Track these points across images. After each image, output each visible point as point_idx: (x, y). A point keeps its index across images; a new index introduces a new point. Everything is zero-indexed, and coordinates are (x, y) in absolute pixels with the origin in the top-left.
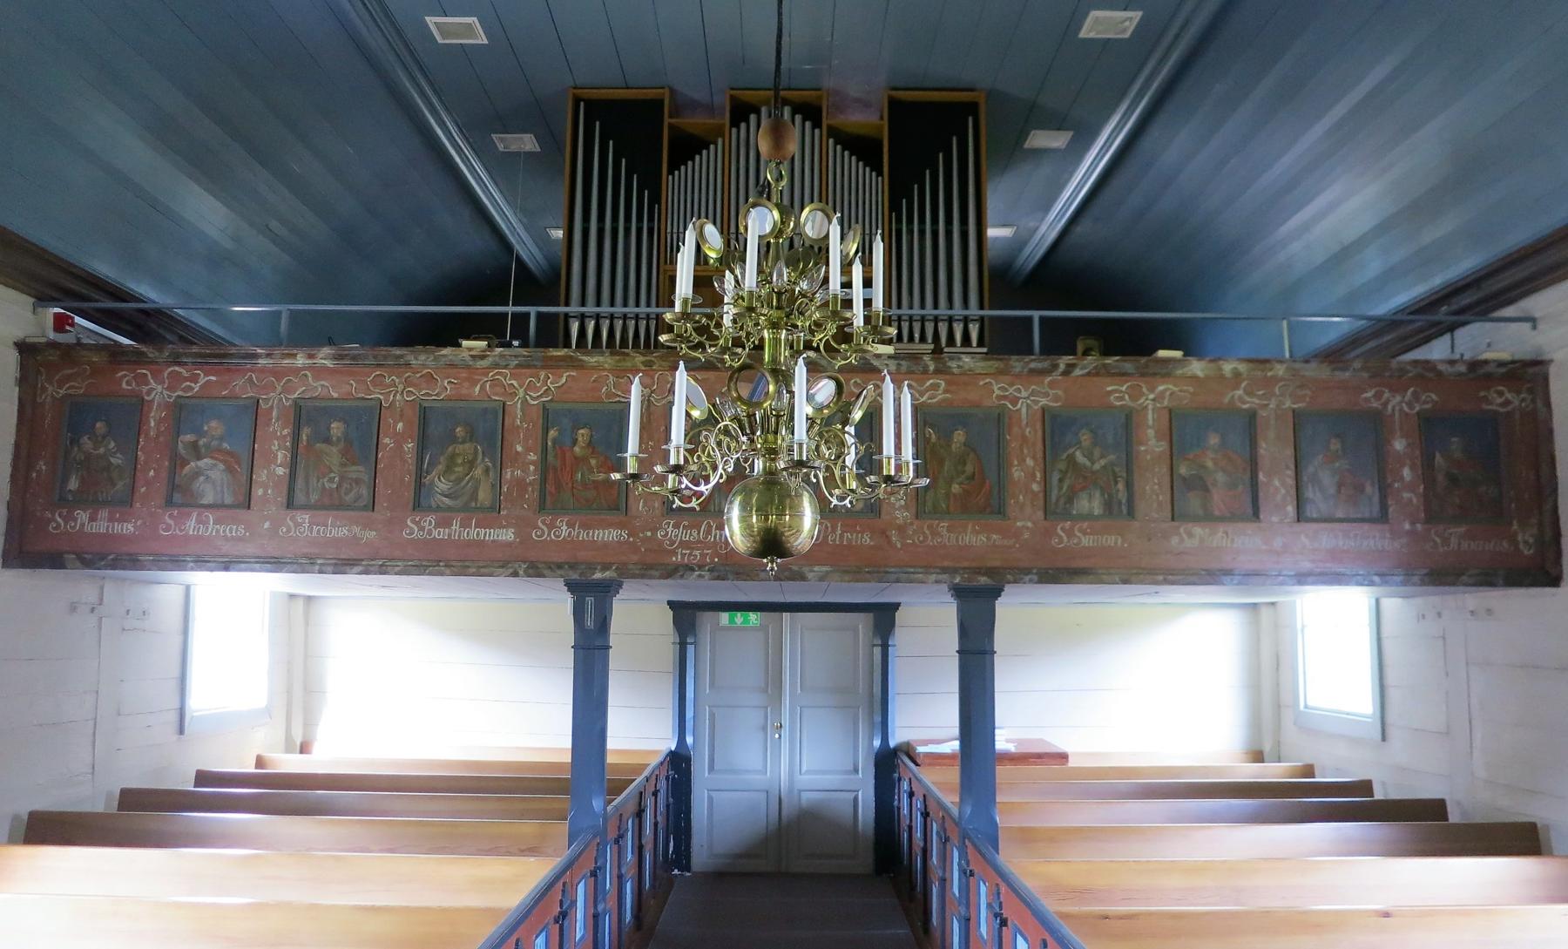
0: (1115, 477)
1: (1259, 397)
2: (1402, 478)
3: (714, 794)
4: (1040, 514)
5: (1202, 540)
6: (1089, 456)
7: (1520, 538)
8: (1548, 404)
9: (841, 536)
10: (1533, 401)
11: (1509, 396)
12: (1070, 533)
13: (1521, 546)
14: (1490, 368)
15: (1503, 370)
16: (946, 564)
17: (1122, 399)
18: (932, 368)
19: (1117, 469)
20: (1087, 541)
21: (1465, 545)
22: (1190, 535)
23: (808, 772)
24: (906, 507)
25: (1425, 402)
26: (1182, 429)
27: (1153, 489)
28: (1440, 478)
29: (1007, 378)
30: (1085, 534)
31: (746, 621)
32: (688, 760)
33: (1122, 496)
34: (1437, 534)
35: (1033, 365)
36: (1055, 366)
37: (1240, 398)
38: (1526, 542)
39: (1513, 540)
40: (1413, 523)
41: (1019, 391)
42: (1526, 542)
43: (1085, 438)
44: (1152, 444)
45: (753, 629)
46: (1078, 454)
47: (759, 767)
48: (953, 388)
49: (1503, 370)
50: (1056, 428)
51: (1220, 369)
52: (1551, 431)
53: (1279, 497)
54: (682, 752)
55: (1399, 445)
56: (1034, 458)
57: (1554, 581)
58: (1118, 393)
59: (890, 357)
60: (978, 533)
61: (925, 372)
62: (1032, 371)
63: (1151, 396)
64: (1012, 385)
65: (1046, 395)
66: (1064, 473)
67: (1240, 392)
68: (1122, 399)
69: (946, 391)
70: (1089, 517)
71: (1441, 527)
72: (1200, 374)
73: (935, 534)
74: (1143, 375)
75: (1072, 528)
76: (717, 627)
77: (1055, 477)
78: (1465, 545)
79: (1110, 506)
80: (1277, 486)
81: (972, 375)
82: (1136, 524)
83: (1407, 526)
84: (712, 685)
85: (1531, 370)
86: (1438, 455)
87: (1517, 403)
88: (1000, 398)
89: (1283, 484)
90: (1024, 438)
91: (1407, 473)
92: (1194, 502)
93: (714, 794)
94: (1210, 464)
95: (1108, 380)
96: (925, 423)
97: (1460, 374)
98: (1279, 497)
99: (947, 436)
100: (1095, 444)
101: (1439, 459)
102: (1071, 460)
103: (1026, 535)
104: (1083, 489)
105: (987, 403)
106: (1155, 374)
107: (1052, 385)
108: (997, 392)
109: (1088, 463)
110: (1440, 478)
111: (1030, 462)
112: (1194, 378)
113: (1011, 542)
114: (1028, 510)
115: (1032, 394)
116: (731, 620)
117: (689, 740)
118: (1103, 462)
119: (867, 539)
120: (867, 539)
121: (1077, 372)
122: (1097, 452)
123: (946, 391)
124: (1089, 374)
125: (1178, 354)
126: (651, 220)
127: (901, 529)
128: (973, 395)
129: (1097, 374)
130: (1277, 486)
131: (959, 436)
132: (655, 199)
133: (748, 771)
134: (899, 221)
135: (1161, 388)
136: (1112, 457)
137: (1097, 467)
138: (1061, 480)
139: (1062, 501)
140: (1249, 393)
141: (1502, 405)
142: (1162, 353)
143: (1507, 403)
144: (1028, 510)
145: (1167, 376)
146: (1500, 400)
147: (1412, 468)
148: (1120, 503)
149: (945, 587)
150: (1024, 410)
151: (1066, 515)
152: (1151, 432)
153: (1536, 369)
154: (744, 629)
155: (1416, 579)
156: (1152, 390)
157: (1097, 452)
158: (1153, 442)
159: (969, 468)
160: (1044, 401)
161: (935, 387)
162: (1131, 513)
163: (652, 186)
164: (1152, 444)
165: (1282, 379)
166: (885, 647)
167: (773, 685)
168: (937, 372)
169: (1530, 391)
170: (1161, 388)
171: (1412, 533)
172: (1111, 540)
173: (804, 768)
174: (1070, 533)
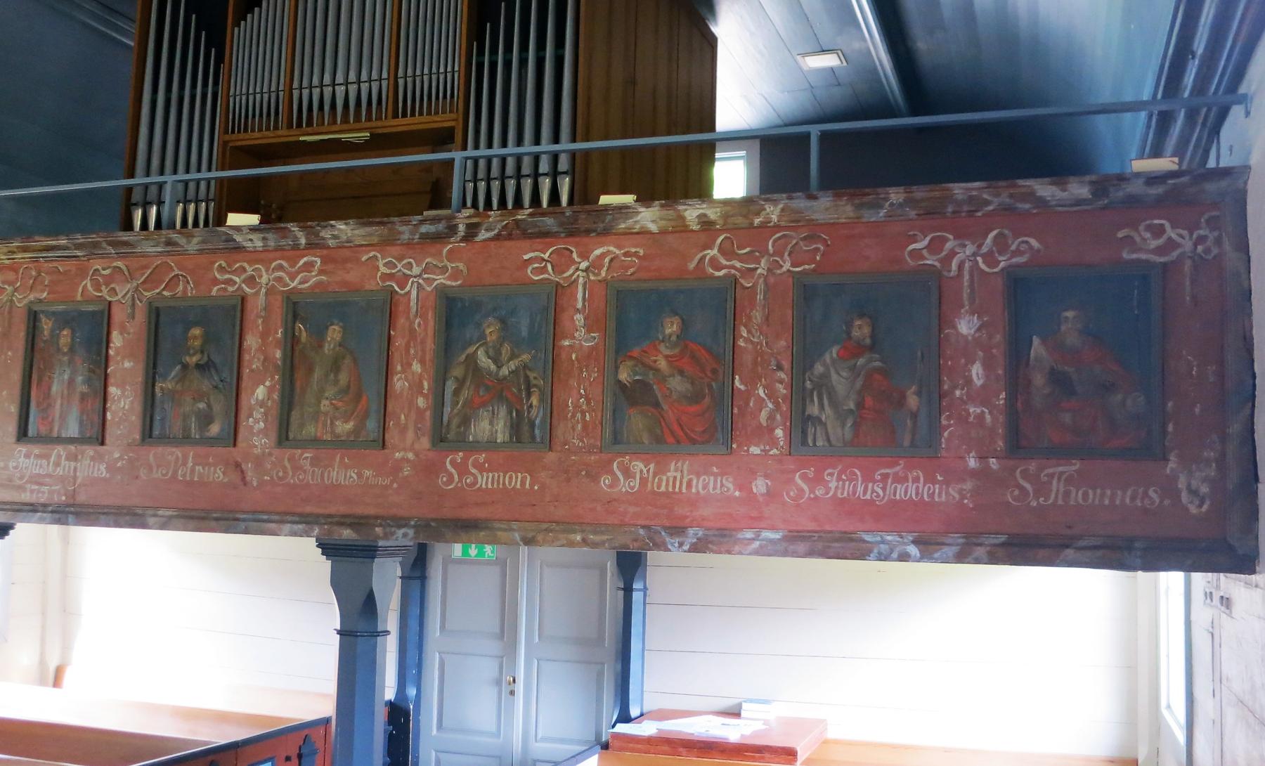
0: (529, 387)
1: (741, 259)
2: (969, 381)
3: (442, 756)
4: (425, 442)
5: (643, 481)
6: (496, 360)
7: (1182, 483)
8: (1243, 247)
9: (193, 471)
10: (1218, 242)
11: (1171, 233)
12: (462, 470)
13: (1184, 497)
14: (1136, 188)
15: (1158, 190)
16: (308, 509)
17: (543, 270)
18: (303, 241)
19: (532, 375)
20: (484, 481)
21: (1077, 496)
22: (628, 474)
23: (544, 739)
24: (264, 432)
25: (1018, 253)
26: (631, 312)
27: (582, 400)
28: (1039, 380)
29: (395, 250)
30: (481, 468)
31: (481, 553)
32: (406, 714)
33: (537, 414)
34: (1025, 475)
35: (424, 229)
36: (453, 229)
37: (713, 259)
38: (1193, 492)
39: (1170, 490)
40: (982, 458)
41: (410, 266)
42: (1193, 492)
43: (491, 330)
44: (580, 336)
45: (488, 563)
46: (481, 353)
47: (493, 729)
48: (330, 267)
49: (1158, 190)
50: (454, 313)
51: (683, 218)
52: (1247, 295)
53: (764, 415)
54: (403, 705)
55: (966, 326)
56: (422, 362)
57: (1242, 562)
58: (537, 263)
59: (253, 229)
60: (347, 467)
61: (296, 247)
62: (424, 237)
63: (584, 265)
64: (400, 259)
65: (444, 270)
66: (461, 383)
67: (714, 252)
68: (543, 270)
69: (321, 272)
70: (491, 445)
71: (1033, 466)
72: (653, 228)
73: (297, 468)
74: (571, 234)
75: (465, 459)
76: (448, 561)
77: (450, 386)
78: (1077, 496)
79: (518, 429)
80: (765, 401)
81: (347, 245)
82: (551, 457)
83: (972, 463)
84: (443, 627)
85: (1211, 187)
86: (1036, 341)
87: (1188, 245)
88: (386, 277)
89: (771, 395)
90: (412, 331)
91: (976, 371)
92: (637, 421)
93: (442, 756)
94: (662, 364)
95: (526, 244)
96: (295, 317)
97: (1079, 202)
98: (764, 415)
99: (319, 334)
100: (501, 340)
101: (1037, 348)
102: (472, 359)
103: (407, 471)
104: (484, 404)
105: (370, 285)
106: (588, 232)
107: (452, 255)
108: (383, 269)
109: (493, 367)
110: (1039, 380)
111: (416, 367)
112: (644, 232)
113: (387, 482)
114: (410, 435)
115: (425, 271)
116: (464, 552)
117: (411, 692)
118: (512, 365)
119: (218, 475)
120: (218, 475)
121: (483, 235)
122: (506, 350)
123: (321, 272)
124: (497, 238)
125: (628, 199)
126: (216, 83)
127: (259, 462)
128: (352, 275)
129: (510, 237)
130: (765, 401)
131: (334, 333)
132: (220, 59)
133: (481, 733)
134: (481, 52)
135: (598, 252)
136: (525, 357)
137: (505, 371)
138: (457, 392)
139: (455, 421)
140: (726, 252)
141: (1160, 251)
142: (605, 199)
143: (1171, 245)
144: (410, 435)
145: (606, 232)
146: (1154, 244)
147: (987, 367)
148: (532, 425)
149: (312, 542)
150: (414, 293)
151: (461, 443)
152: (579, 319)
153: (1224, 184)
154: (478, 563)
155: (980, 552)
156: (585, 256)
157: (506, 350)
158: (581, 333)
159: (343, 378)
160: (441, 279)
161: (309, 265)
162: (550, 442)
163: (218, 42)
164: (580, 336)
165: (778, 228)
166: (628, 591)
167: (506, 632)
168: (311, 246)
169: (1213, 224)
170: (598, 252)
171: (981, 474)
172: (516, 480)
173: (539, 736)
174: (462, 470)
